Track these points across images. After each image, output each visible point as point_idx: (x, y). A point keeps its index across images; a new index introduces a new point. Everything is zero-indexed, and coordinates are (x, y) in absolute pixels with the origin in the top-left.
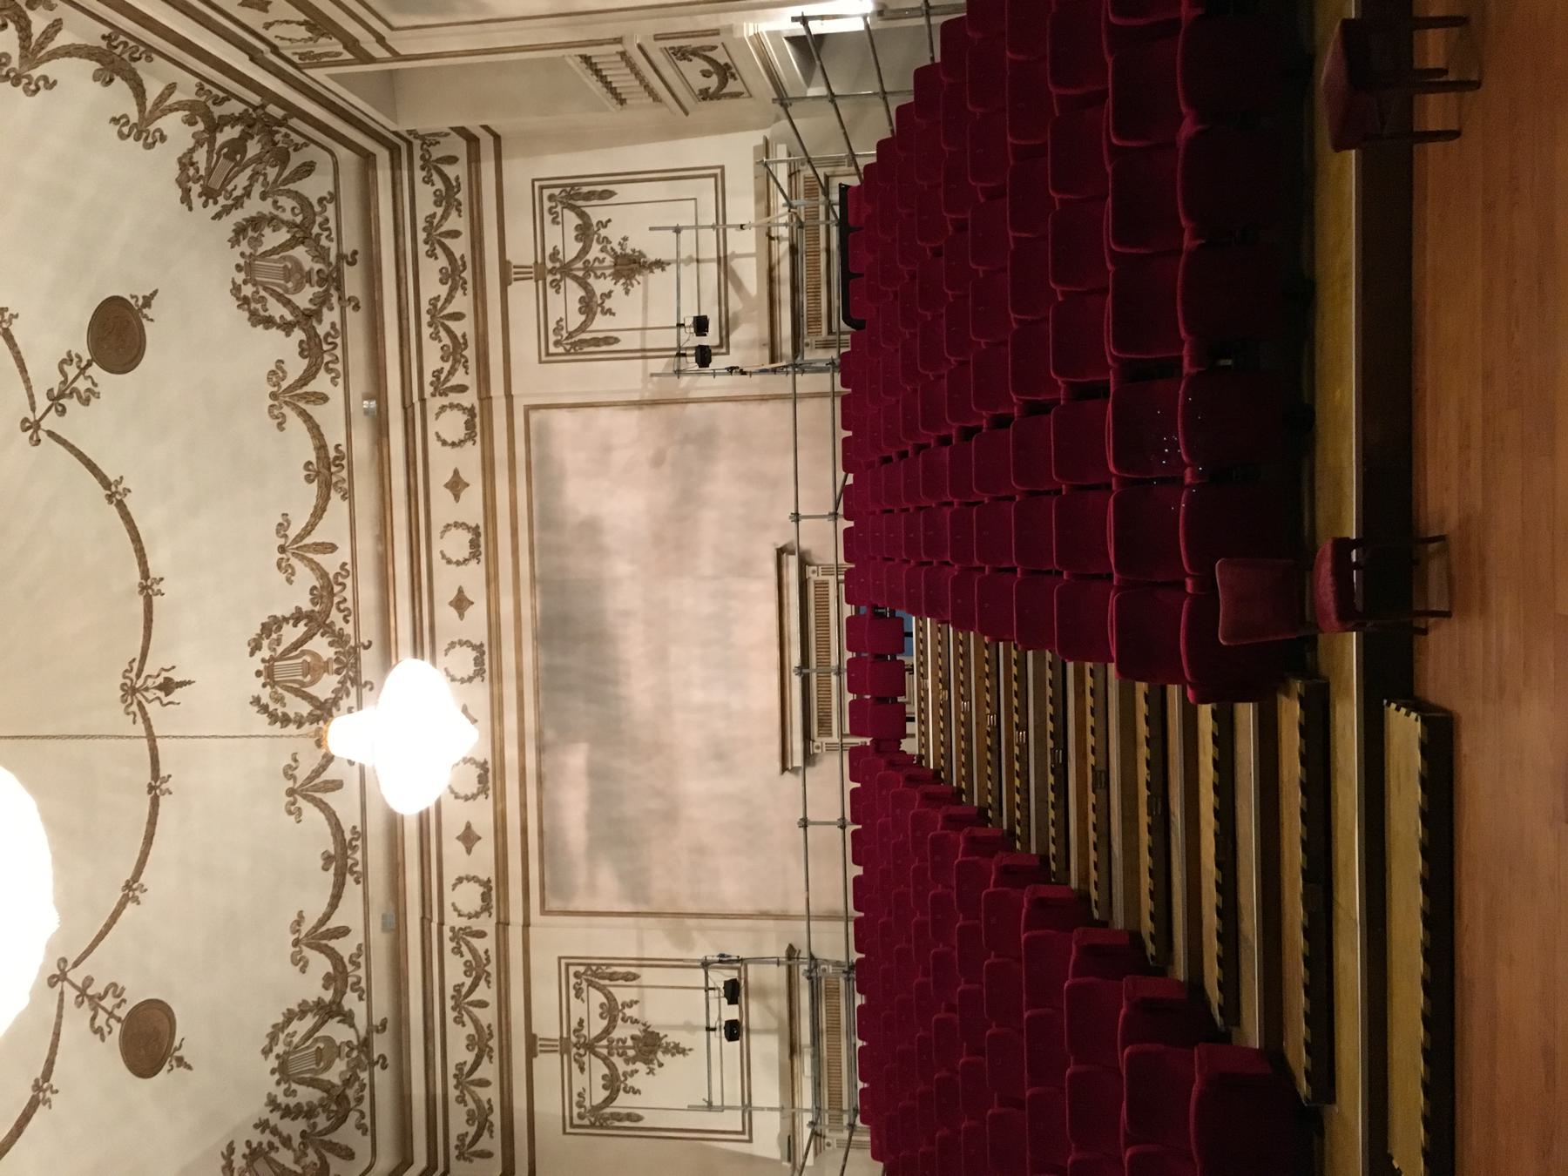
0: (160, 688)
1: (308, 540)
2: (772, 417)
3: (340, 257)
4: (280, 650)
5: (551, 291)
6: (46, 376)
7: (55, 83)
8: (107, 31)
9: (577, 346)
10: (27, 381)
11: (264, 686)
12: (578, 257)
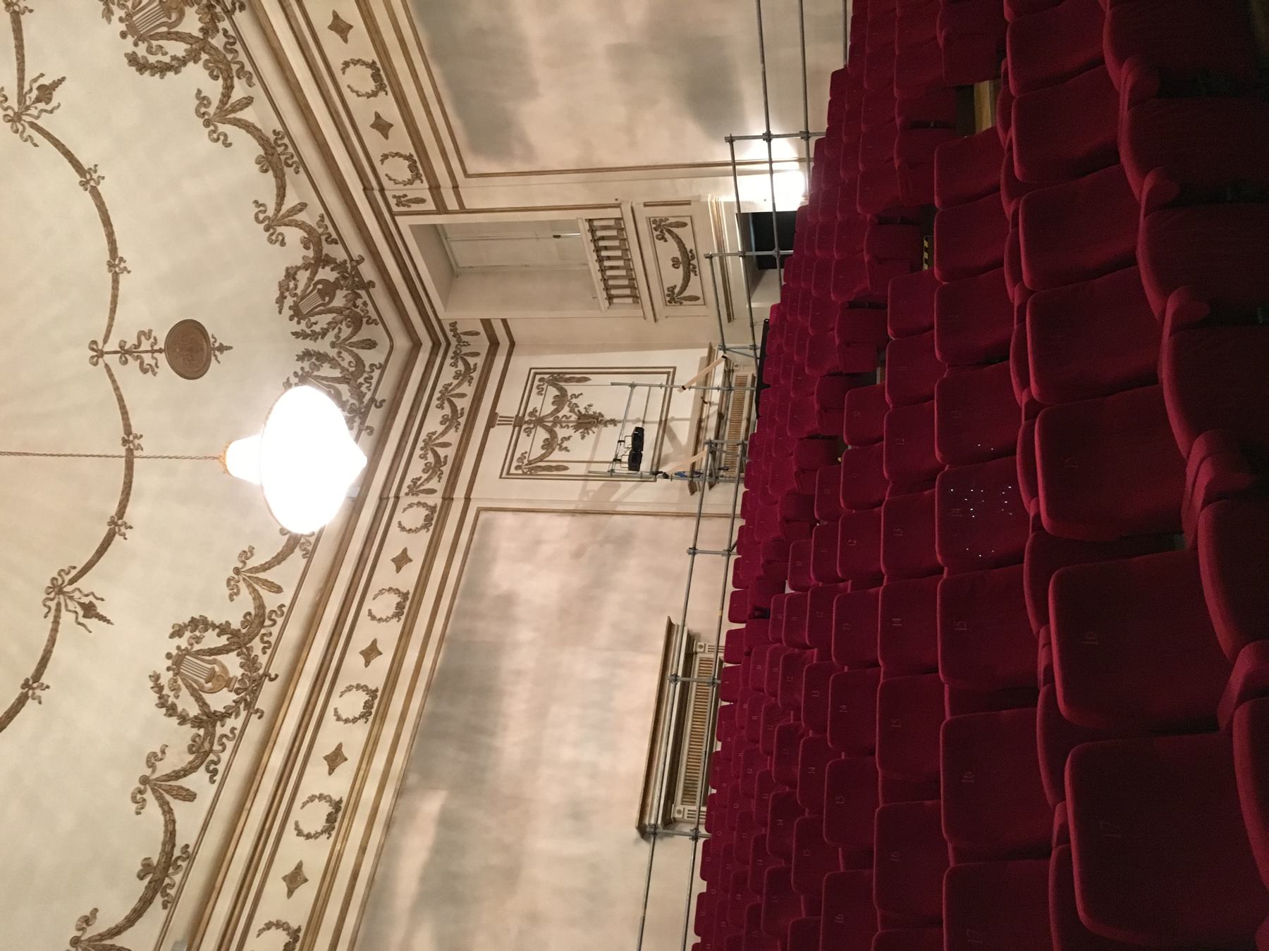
0: (82, 605)
1: (261, 575)
2: (681, 531)
3: (372, 400)
4: (197, 647)
5: (523, 434)
6: (126, 332)
7: (230, 144)
8: (279, 128)
9: (533, 469)
10: (112, 318)
11: (168, 669)
12: (552, 414)
